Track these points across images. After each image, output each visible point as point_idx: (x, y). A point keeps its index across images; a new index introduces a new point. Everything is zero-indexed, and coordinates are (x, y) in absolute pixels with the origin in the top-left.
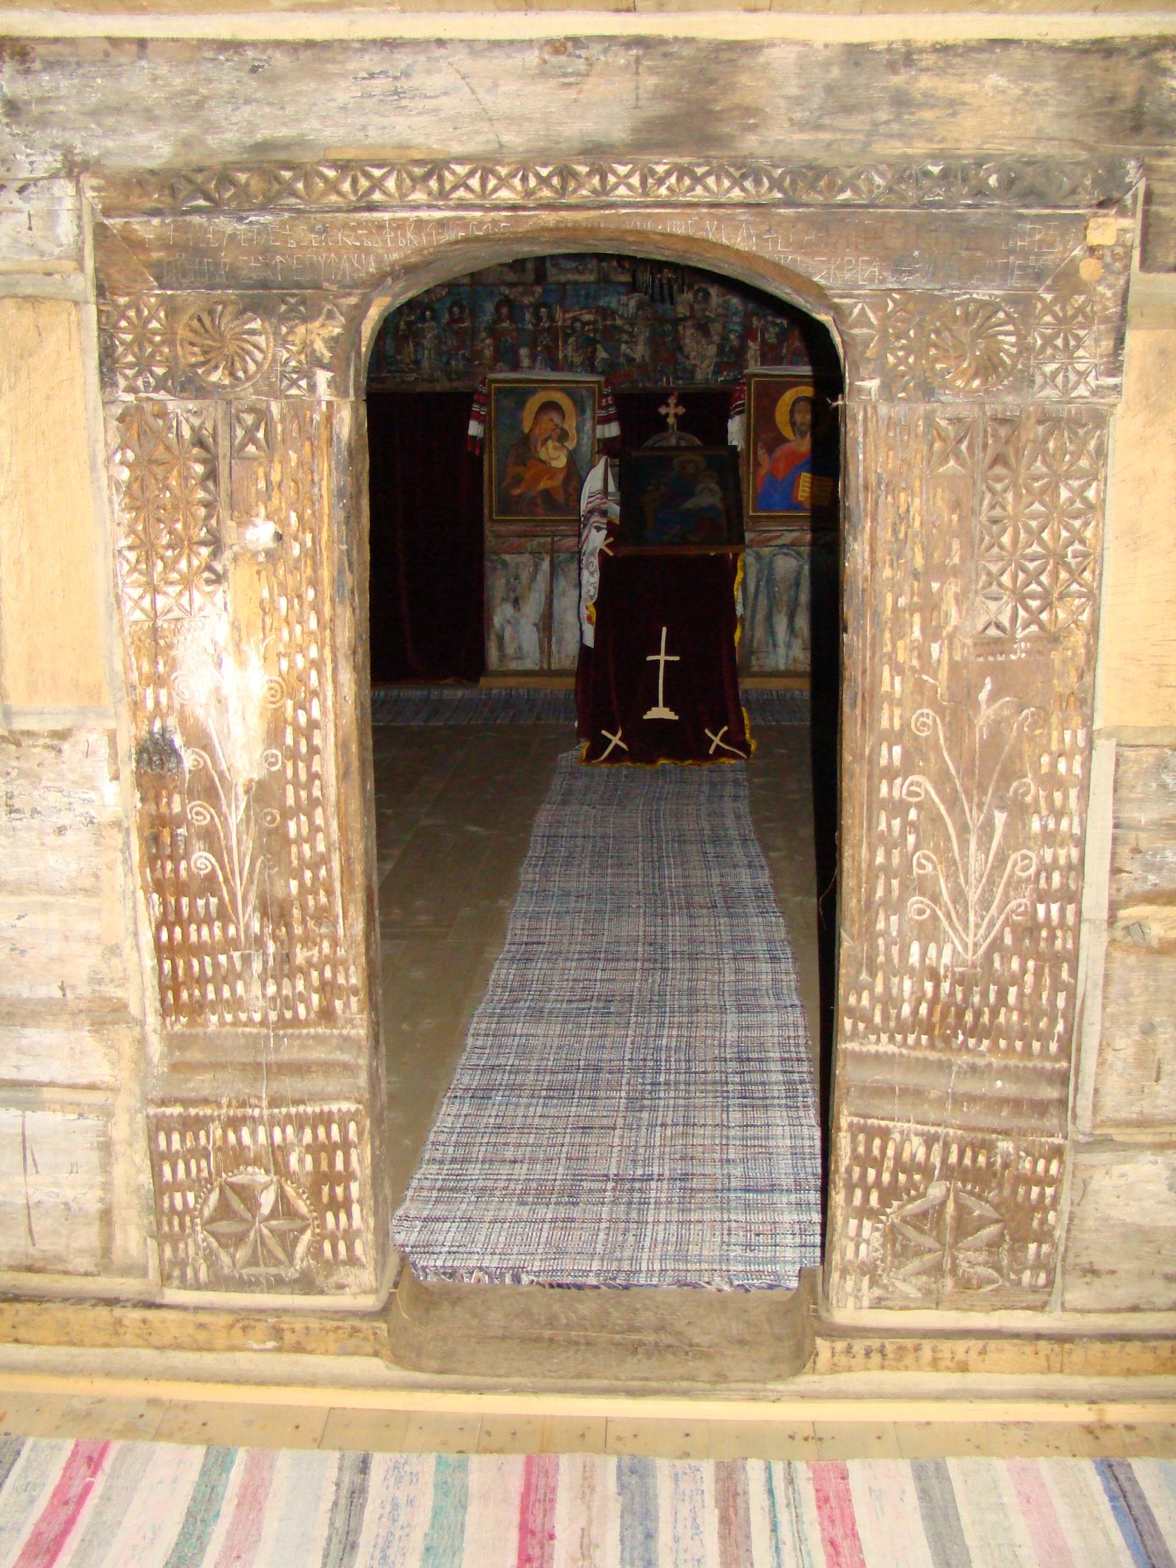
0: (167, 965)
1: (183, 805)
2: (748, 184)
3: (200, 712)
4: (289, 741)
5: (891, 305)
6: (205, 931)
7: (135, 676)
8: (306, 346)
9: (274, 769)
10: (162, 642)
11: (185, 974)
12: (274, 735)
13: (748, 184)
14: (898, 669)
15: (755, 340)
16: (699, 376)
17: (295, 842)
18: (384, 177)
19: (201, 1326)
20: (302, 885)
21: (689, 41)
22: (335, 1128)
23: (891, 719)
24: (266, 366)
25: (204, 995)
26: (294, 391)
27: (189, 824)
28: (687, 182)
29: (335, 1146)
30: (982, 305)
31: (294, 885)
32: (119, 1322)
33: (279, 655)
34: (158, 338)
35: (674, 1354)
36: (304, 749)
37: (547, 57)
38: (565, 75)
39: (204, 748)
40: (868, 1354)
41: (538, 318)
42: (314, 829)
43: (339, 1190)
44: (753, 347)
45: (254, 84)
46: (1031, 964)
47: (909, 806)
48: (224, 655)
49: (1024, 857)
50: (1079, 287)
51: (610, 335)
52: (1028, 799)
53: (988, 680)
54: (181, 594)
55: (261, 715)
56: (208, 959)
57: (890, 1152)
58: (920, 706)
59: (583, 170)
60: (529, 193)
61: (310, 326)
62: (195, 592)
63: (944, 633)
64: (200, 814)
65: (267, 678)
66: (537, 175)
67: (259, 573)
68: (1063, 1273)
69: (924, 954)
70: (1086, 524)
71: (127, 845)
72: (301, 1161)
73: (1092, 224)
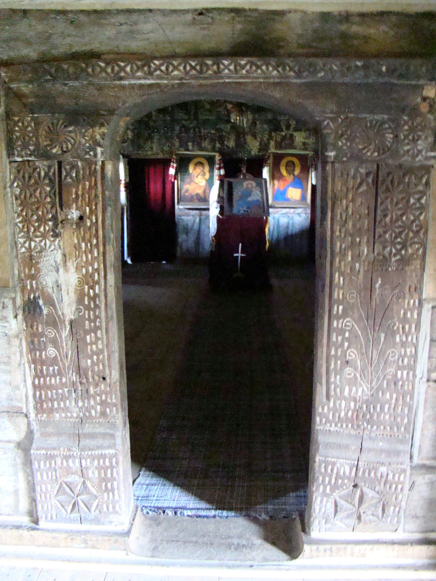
0: (38, 393)
1: (43, 329)
2: (280, 69)
3: (50, 291)
4: (86, 303)
5: (340, 120)
6: (53, 380)
7: (23, 275)
8: (92, 138)
9: (81, 314)
10: (34, 261)
11: (45, 397)
12: (80, 301)
13: (280, 69)
14: (341, 274)
15: (273, 141)
16: (253, 153)
17: (89, 344)
18: (125, 66)
19: (54, 538)
20: (93, 362)
21: (256, 10)
22: (107, 460)
23: (338, 295)
24: (76, 146)
25: (53, 406)
26: (87, 156)
27: (46, 337)
28: (254, 68)
29: (108, 468)
30: (377, 121)
31: (89, 361)
32: (21, 535)
33: (82, 267)
34: (31, 135)
35: (246, 548)
36: (92, 306)
37: (196, 17)
38: (202, 24)
39: (52, 306)
40: (325, 551)
41: (194, 130)
42: (97, 339)
43: (109, 485)
44: (272, 143)
45: (72, 28)
46: (394, 396)
47: (345, 331)
48: (60, 267)
49: (393, 352)
50: (420, 114)
51: (221, 139)
52: (395, 328)
53: (380, 279)
54: (41, 241)
55: (75, 292)
56: (54, 391)
57: (335, 471)
58: (350, 289)
59: (209, 62)
60: (187, 73)
61: (94, 129)
62: (47, 240)
63: (362, 259)
64: (51, 333)
65: (77, 276)
66: (191, 65)
67: (73, 233)
68: (404, 517)
69: (350, 391)
70: (421, 214)
71: (21, 344)
72: (93, 473)
73: (425, 87)
